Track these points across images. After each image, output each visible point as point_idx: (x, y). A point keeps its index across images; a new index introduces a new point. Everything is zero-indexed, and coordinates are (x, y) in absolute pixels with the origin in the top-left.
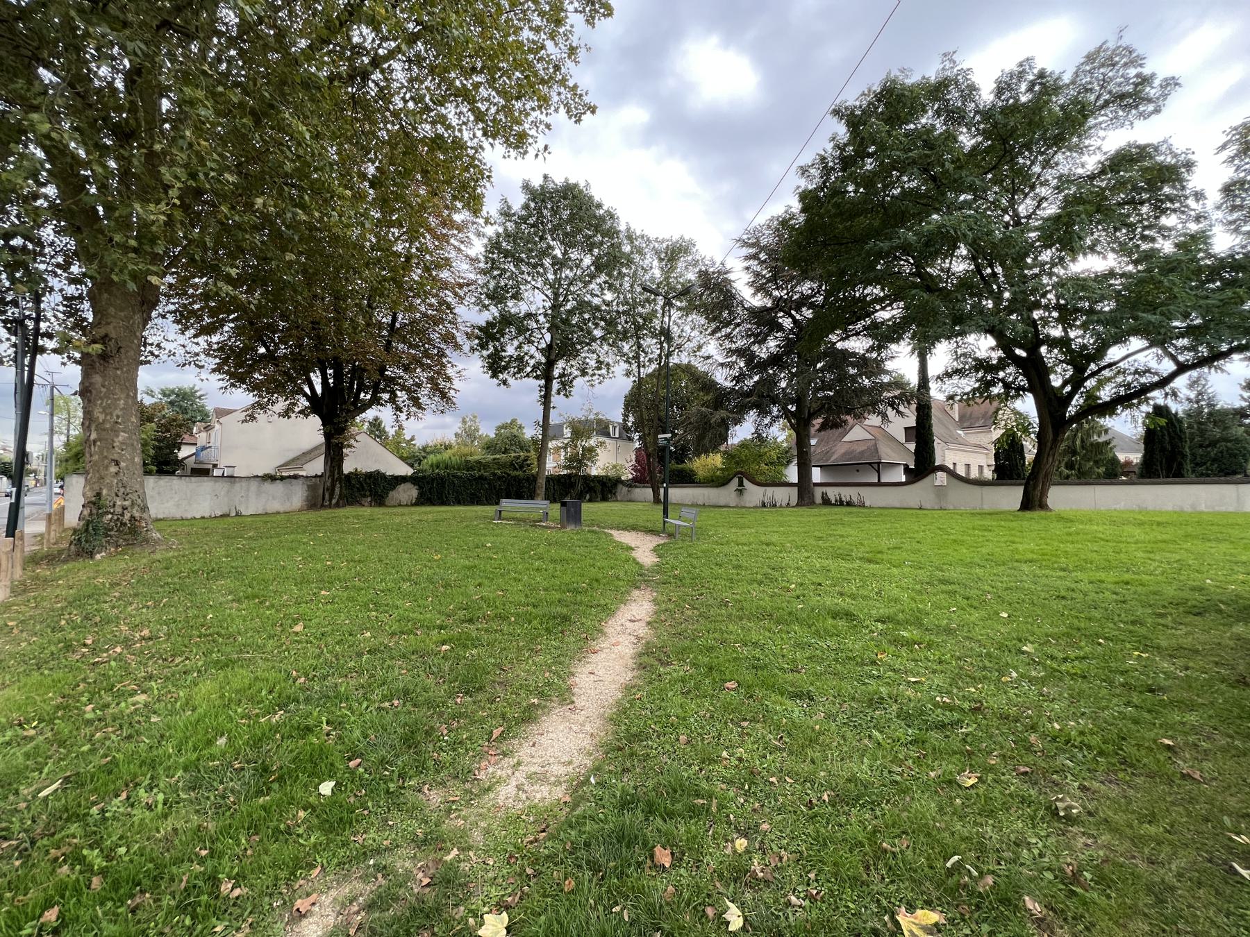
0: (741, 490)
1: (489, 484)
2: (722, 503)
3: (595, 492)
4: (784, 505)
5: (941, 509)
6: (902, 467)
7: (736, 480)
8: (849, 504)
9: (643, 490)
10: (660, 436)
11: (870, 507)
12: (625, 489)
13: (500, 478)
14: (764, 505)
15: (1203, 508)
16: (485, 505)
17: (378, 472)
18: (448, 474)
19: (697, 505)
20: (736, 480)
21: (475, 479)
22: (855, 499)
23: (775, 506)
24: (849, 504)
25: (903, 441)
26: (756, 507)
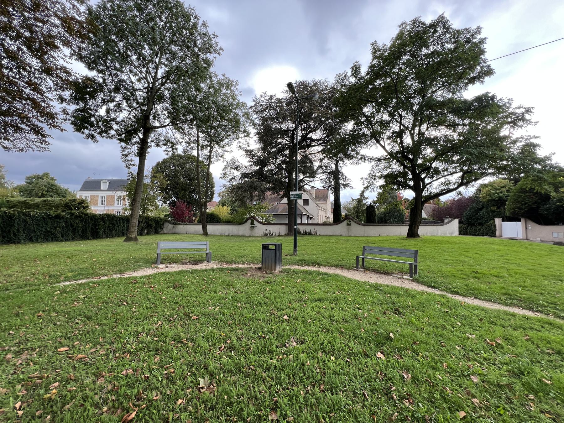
0: (253, 226)
1: (66, 222)
2: (240, 234)
3: (151, 227)
4: (277, 234)
5: (349, 236)
6: (306, 216)
7: (249, 221)
8: (310, 234)
9: (185, 226)
10: (291, 193)
11: (320, 236)
12: (171, 226)
13: (77, 217)
14: (266, 235)
15: (429, 234)
16: (61, 241)
17: (158, 164)
18: (19, 212)
19: (225, 236)
20: (249, 221)
21: (50, 218)
22: (313, 232)
23: (272, 235)
24: (310, 234)
25: (302, 205)
26: (261, 236)
